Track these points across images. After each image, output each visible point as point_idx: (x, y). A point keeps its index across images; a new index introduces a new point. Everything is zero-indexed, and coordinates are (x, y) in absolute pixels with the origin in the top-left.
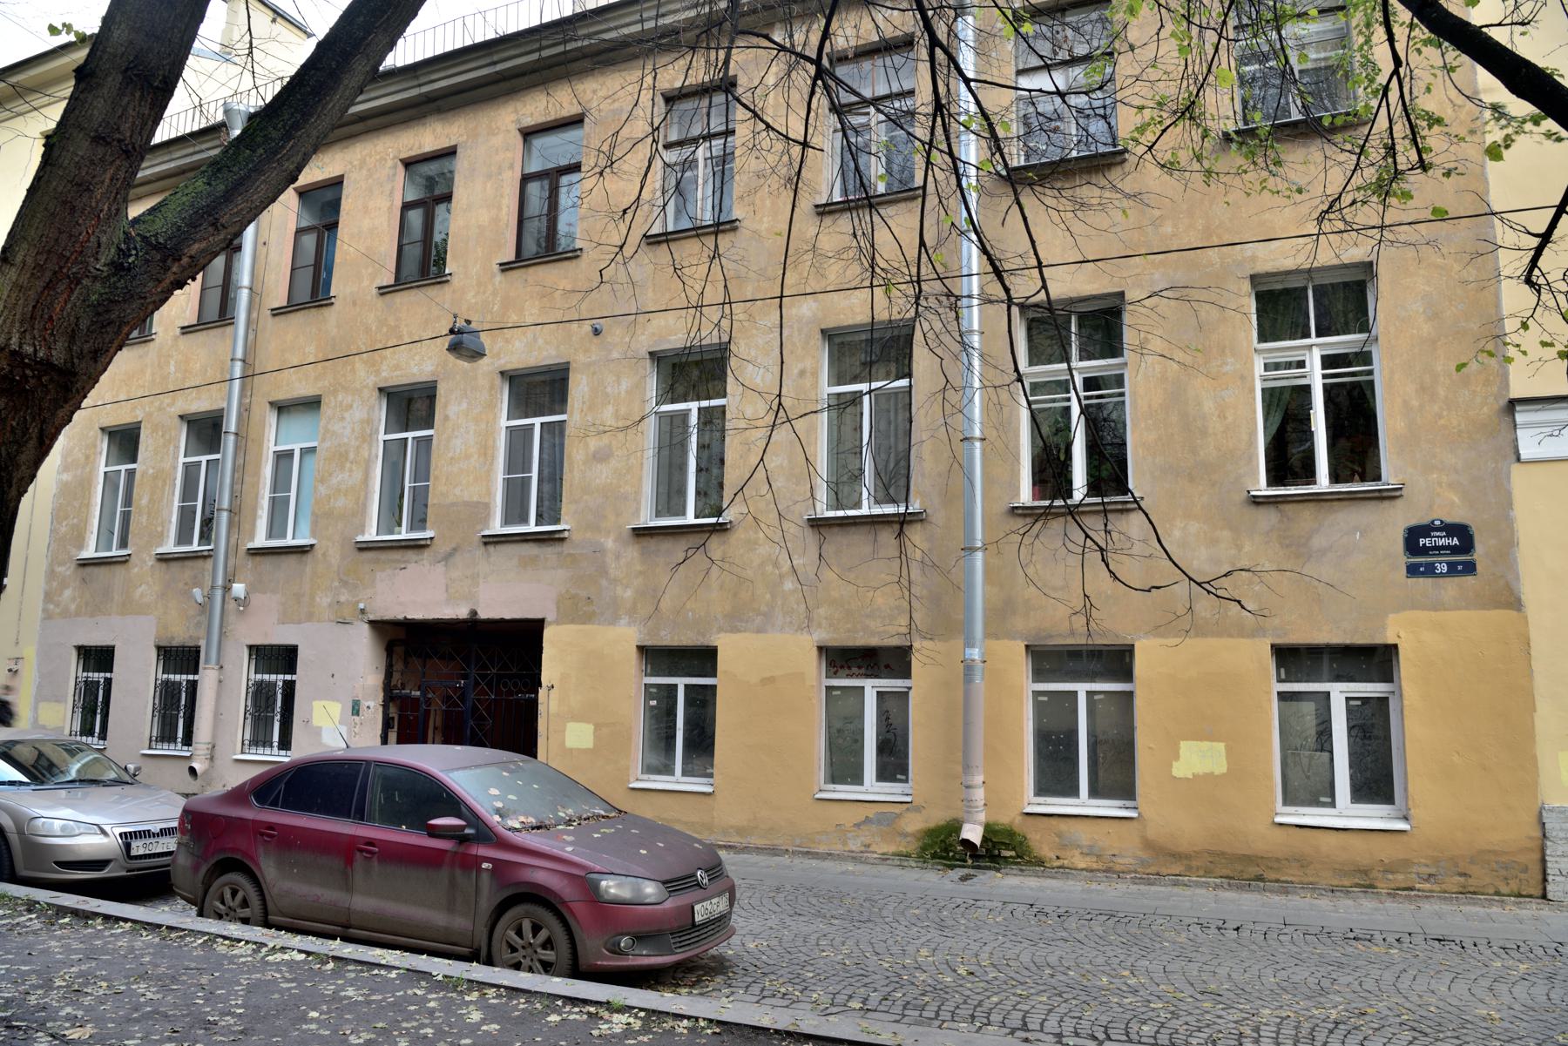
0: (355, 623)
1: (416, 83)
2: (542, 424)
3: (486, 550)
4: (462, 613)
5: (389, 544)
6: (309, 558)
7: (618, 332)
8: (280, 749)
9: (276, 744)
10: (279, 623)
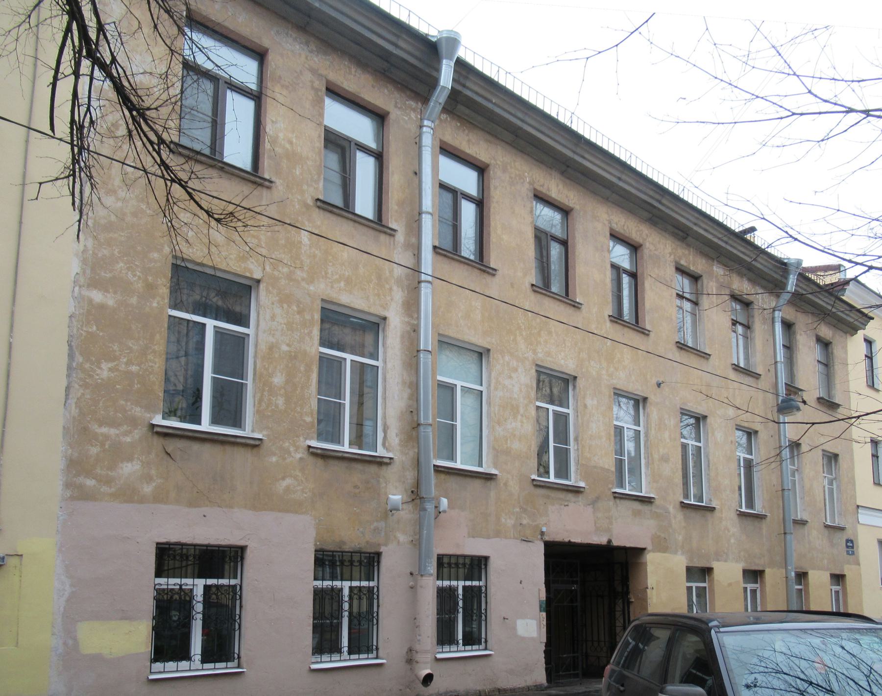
0: (536, 542)
1: (574, 149)
2: (640, 431)
3: (616, 502)
4: (602, 540)
5: (561, 487)
6: (492, 484)
7: (667, 390)
8: (464, 645)
9: (461, 642)
10: (469, 537)
